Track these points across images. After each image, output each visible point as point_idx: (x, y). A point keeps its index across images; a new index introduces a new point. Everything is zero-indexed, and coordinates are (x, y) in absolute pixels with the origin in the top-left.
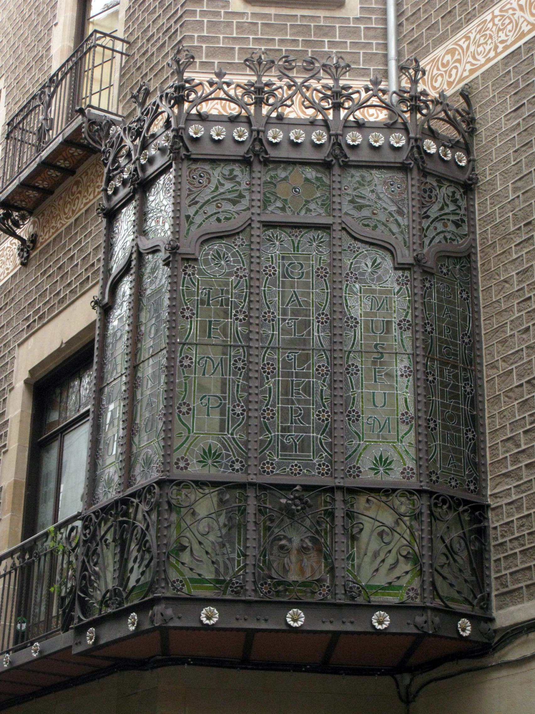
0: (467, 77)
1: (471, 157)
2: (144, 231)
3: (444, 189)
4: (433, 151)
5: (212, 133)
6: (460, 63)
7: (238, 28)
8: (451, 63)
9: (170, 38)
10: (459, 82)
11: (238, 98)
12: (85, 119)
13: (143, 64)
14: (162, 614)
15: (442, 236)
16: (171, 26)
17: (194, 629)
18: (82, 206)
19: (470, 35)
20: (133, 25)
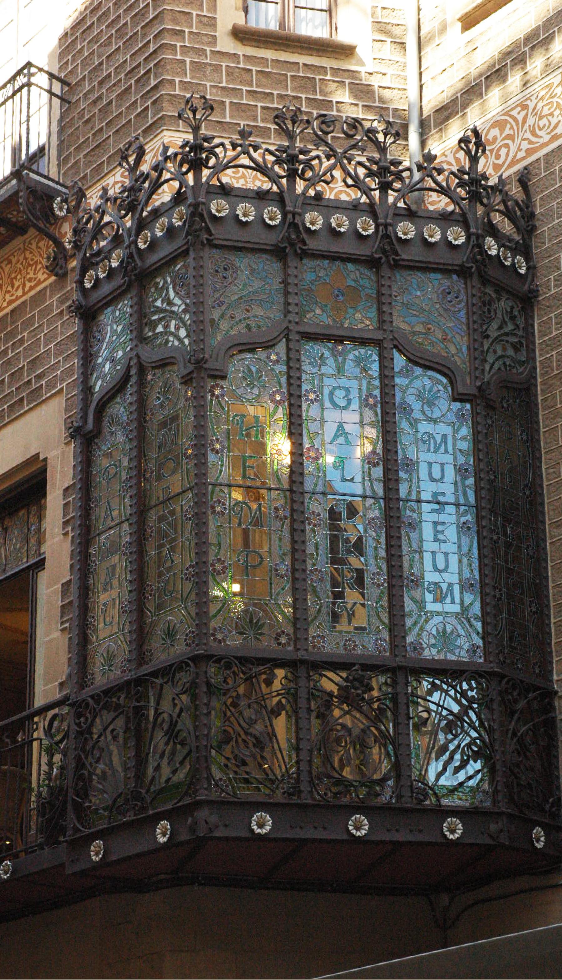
0: (523, 159)
1: (531, 264)
2: (145, 339)
3: (502, 303)
4: (494, 252)
5: (238, 212)
6: (513, 140)
7: (228, 74)
8: (499, 139)
9: (137, 81)
10: (509, 166)
11: (267, 167)
12: (22, 186)
13: (94, 115)
14: (206, 822)
15: (501, 362)
16: (139, 64)
17: (241, 839)
18: (5, 304)
19: (528, 102)
20: (73, 61)
